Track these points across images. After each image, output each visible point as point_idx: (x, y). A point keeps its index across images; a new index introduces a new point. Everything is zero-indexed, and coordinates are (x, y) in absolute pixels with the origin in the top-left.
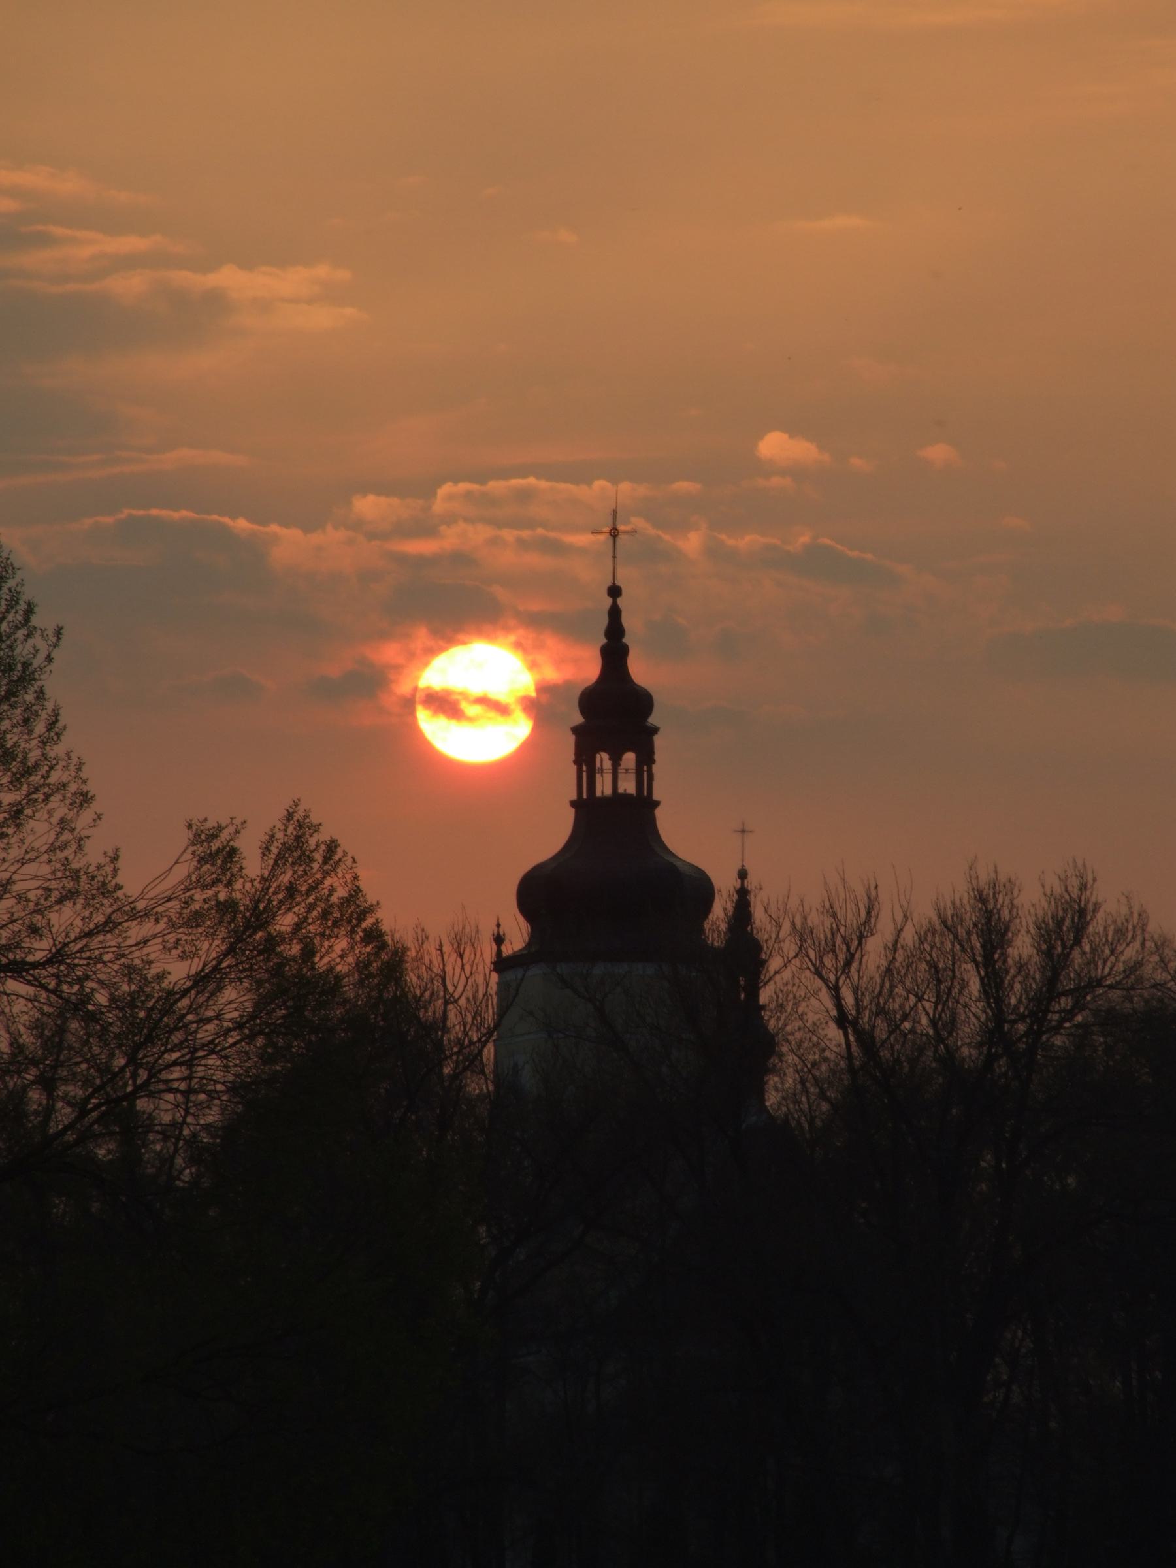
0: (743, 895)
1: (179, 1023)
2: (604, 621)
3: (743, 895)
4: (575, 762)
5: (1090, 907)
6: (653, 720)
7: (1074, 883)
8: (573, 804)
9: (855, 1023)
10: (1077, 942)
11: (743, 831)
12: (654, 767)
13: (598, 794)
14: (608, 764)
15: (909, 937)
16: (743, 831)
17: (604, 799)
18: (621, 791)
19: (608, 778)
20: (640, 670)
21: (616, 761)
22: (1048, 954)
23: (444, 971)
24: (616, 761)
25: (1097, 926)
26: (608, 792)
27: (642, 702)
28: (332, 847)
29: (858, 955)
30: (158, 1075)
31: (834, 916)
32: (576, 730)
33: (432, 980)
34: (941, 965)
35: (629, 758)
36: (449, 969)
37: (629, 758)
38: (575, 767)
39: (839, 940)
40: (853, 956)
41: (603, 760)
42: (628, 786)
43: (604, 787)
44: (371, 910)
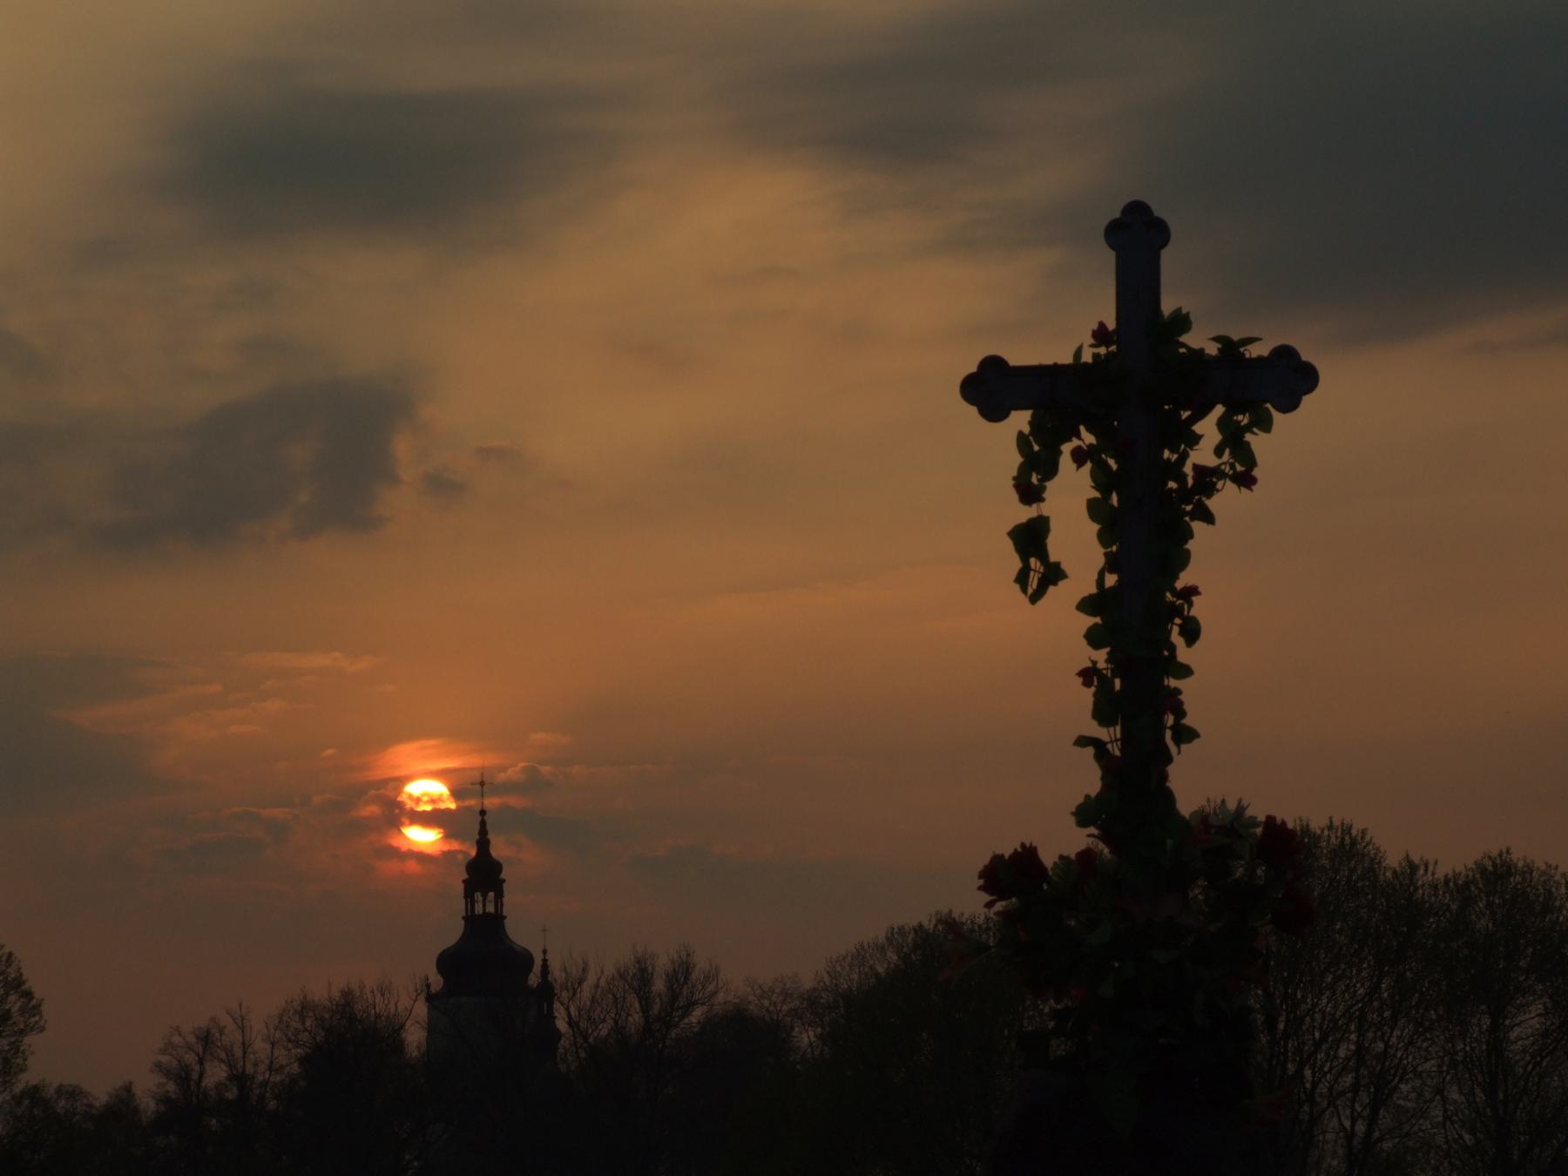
0: (545, 961)
1: (1313, 1035)
2: (478, 827)
3: (545, 961)
4: (464, 897)
5: (691, 965)
6: (503, 876)
7: (684, 954)
8: (463, 918)
9: (577, 1024)
10: (685, 982)
11: (545, 930)
12: (504, 899)
13: (476, 913)
14: (480, 899)
15: (603, 982)
16: (545, 930)
17: (479, 916)
18: (487, 911)
19: (481, 906)
20: (498, 850)
21: (485, 896)
22: (671, 988)
23: (374, 1002)
24: (485, 896)
25: (696, 975)
26: (481, 912)
27: (496, 867)
28: (10, 955)
29: (578, 991)
30: (1354, 1074)
31: (566, 973)
32: (464, 881)
33: (368, 1007)
34: (618, 996)
35: (491, 894)
36: (377, 1001)
37: (491, 894)
38: (464, 901)
39: (569, 984)
40: (576, 991)
41: (478, 896)
42: (491, 909)
43: (479, 909)
44: (24, 983)
